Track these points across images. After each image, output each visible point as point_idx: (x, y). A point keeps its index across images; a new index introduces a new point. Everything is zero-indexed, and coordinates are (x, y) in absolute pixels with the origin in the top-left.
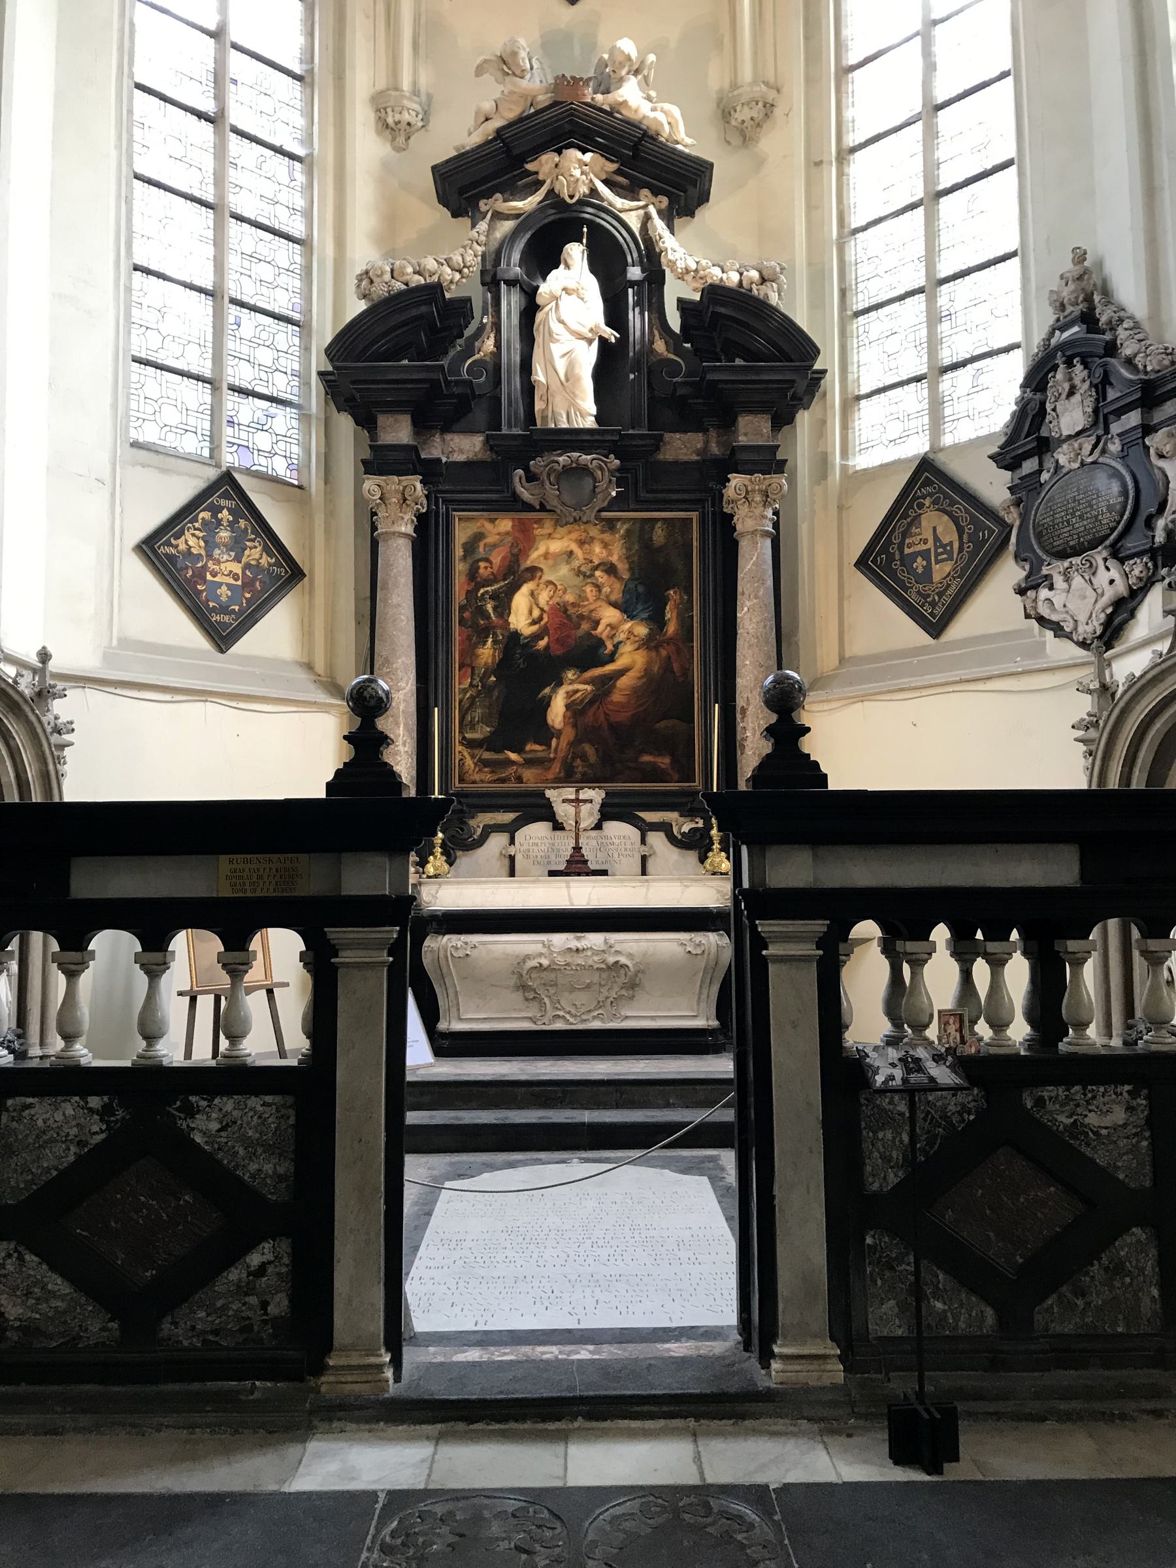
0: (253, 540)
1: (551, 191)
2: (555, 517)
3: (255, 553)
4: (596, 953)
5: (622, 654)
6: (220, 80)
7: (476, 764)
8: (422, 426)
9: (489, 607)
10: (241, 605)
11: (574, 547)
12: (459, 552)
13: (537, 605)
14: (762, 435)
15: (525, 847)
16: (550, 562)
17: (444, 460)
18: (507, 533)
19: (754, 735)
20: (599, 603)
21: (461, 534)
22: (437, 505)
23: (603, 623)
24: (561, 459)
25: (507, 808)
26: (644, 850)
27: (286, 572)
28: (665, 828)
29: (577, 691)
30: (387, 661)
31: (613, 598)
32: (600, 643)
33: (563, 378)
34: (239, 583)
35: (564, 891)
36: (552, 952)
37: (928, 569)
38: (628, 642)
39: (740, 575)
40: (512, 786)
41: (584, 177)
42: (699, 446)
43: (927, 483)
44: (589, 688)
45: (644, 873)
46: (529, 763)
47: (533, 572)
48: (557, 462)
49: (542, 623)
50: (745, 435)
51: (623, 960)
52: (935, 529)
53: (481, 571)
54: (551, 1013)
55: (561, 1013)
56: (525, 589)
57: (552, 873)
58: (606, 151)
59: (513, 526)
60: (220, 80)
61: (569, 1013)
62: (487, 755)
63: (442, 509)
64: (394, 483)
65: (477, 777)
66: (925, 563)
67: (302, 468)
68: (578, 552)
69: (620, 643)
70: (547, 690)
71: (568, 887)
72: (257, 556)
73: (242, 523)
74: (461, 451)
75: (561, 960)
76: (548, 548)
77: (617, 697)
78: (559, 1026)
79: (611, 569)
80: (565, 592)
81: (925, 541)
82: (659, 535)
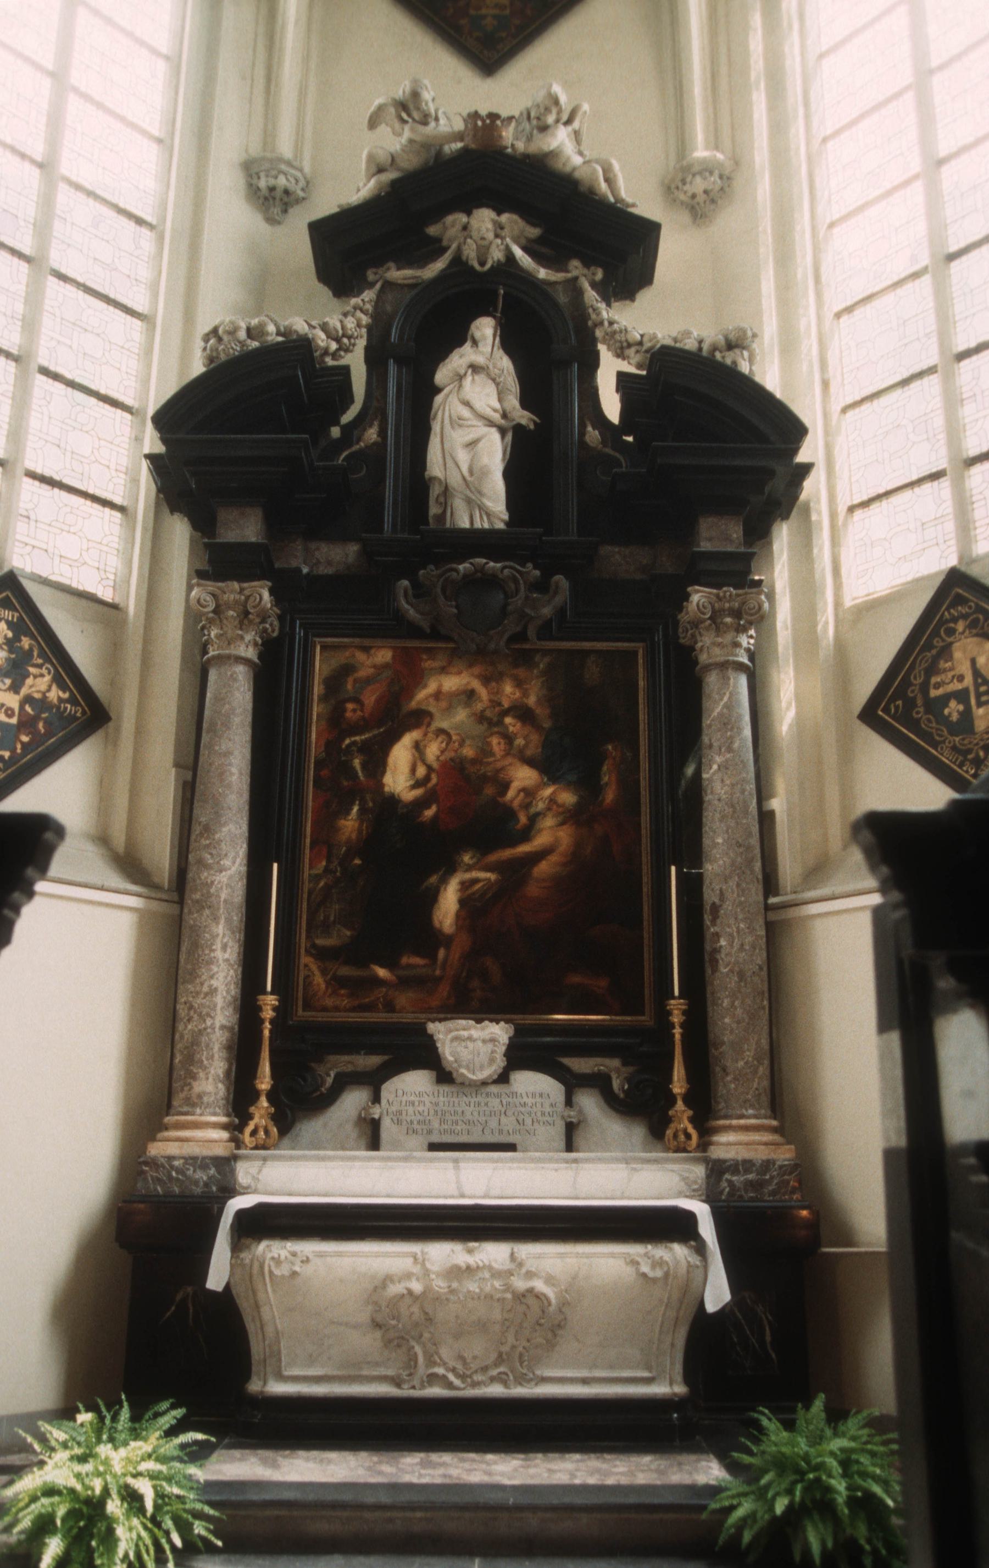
0: (40, 666)
1: (458, 260)
2: (452, 645)
3: (40, 682)
4: (496, 1274)
5: (540, 831)
6: (55, 123)
7: (328, 983)
8: (278, 525)
9: (357, 763)
10: (13, 751)
11: (476, 684)
12: (317, 689)
13: (424, 762)
14: (731, 541)
15: (393, 1109)
16: (444, 704)
17: (305, 570)
18: (386, 666)
19: (731, 945)
20: (510, 760)
21: (321, 666)
22: (293, 628)
23: (516, 785)
24: (461, 567)
25: (372, 1050)
26: (572, 1114)
27: (84, 713)
28: (600, 1083)
29: (476, 881)
30: (207, 829)
31: (529, 753)
32: (509, 813)
33: (466, 473)
34: (14, 721)
35: (451, 1174)
36: (427, 1272)
37: (967, 715)
38: (550, 814)
39: (706, 722)
40: (379, 1017)
41: (499, 241)
42: (645, 562)
43: (960, 600)
44: (492, 876)
45: (570, 1147)
46: (404, 983)
47: (419, 718)
48: (457, 571)
49: (430, 785)
50: (710, 539)
51: (539, 1285)
52: (973, 662)
53: (349, 714)
54: (422, 1370)
55: (440, 1371)
56: (408, 740)
57: (433, 1147)
58: (527, 213)
59: (394, 657)
60: (55, 123)
61: (454, 1370)
62: (345, 971)
63: (299, 632)
64: (232, 592)
65: (329, 1002)
66: (961, 708)
67: (121, 584)
68: (483, 692)
69: (538, 814)
70: (434, 879)
71: (457, 1168)
72: (43, 688)
73: (26, 642)
74: (329, 563)
75: (440, 1285)
76: (440, 686)
77: (533, 890)
78: (436, 1391)
79: (524, 714)
80: (462, 743)
81: (961, 678)
82: (593, 672)
